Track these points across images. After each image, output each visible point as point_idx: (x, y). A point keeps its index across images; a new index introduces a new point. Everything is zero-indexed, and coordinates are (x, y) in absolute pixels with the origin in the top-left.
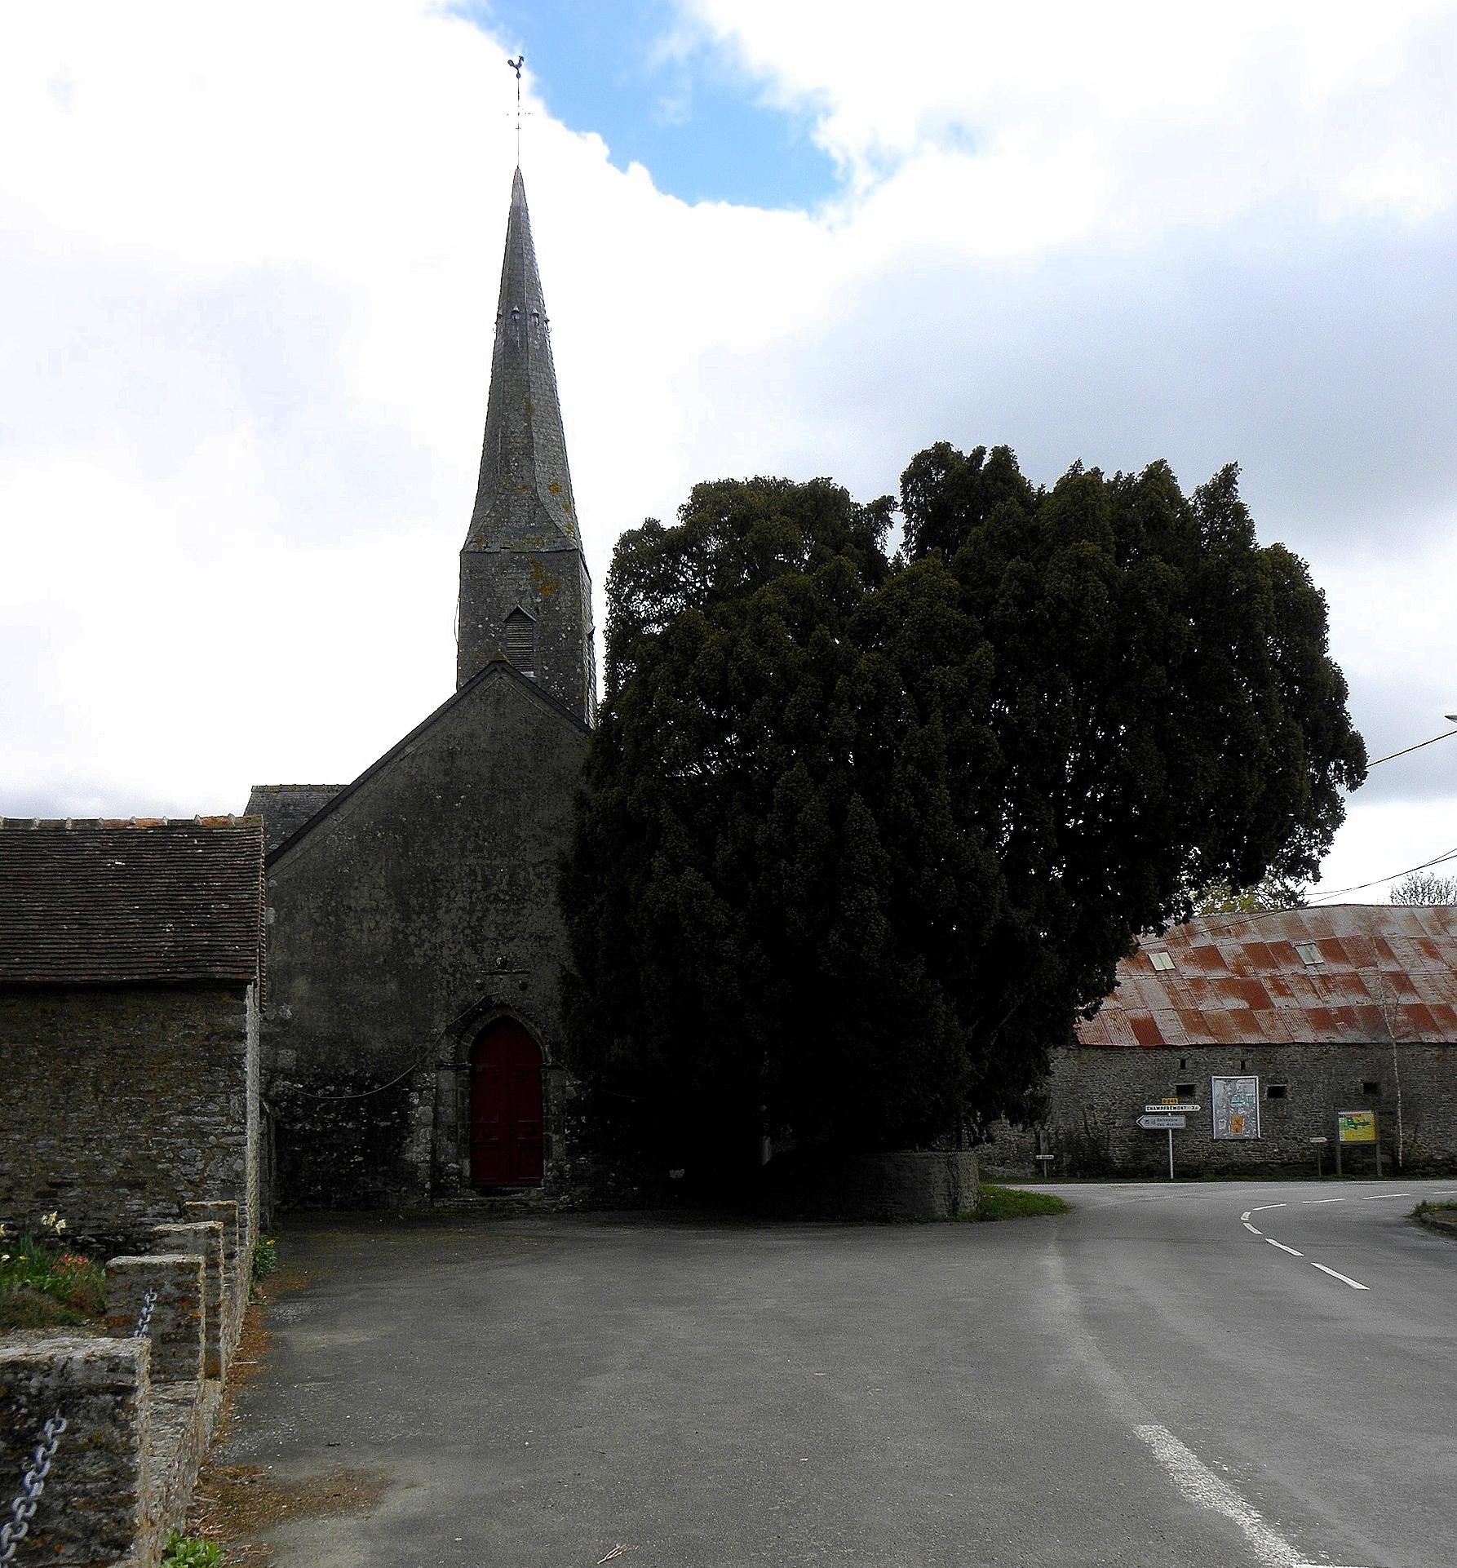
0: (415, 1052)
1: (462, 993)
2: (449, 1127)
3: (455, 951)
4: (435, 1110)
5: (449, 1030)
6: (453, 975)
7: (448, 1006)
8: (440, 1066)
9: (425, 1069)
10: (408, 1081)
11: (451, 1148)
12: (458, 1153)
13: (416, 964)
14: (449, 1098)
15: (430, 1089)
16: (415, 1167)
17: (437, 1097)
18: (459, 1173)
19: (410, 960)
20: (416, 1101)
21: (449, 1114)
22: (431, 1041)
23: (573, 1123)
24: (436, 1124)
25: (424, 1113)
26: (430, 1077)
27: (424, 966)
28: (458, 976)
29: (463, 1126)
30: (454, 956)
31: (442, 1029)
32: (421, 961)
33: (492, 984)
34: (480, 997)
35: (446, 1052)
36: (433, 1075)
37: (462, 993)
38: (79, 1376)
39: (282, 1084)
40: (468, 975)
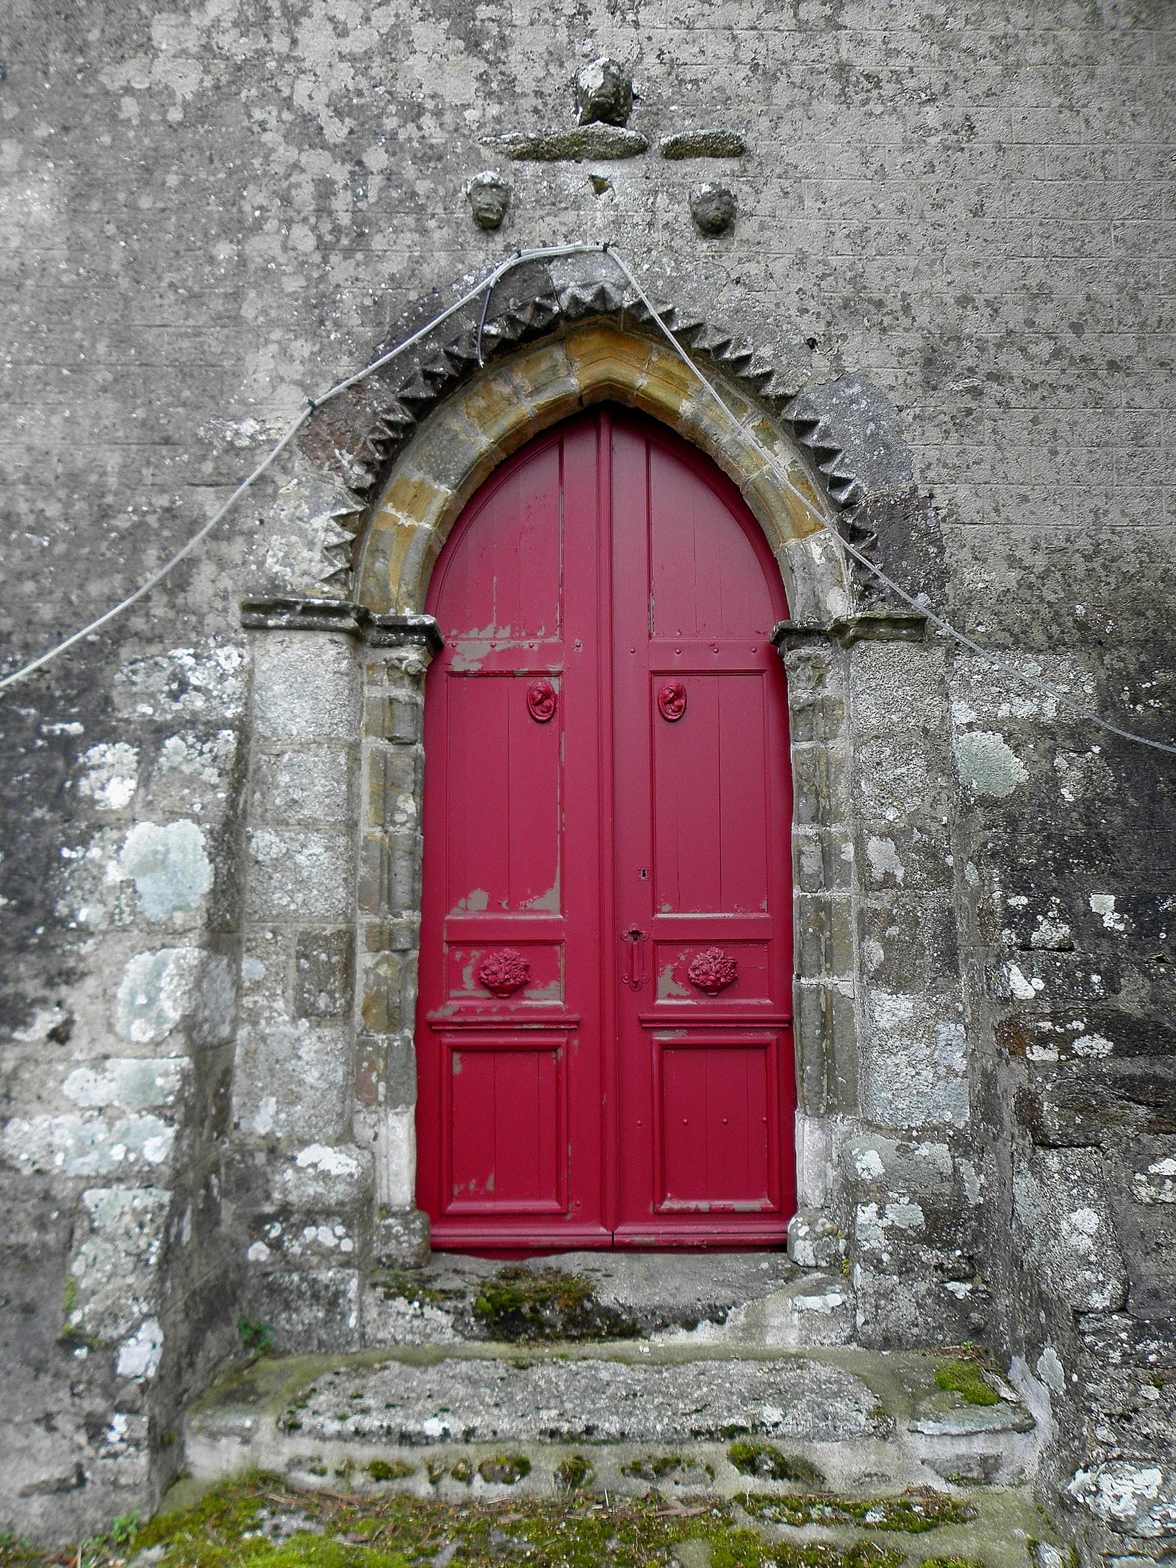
0: (136, 537)
1: (394, 249)
2: (308, 941)
3: (361, 40)
4: (228, 840)
5: (322, 427)
6: (351, 154)
7: (318, 309)
8: (267, 610)
9: (187, 627)
10: (84, 691)
11: (314, 1057)
12: (357, 1088)
13: (157, 96)
14: (307, 781)
15: (209, 730)
16: (62, 1216)
17: (240, 772)
18: (361, 1209)
19: (132, 73)
20: (117, 793)
21: (306, 872)
22: (220, 482)
23: (1049, 932)
24: (225, 927)
25: (155, 863)
26: (217, 668)
27: (201, 112)
28: (376, 158)
29: (382, 940)
30: (359, 61)
31: (287, 417)
32: (187, 82)
33: (555, 201)
34: (486, 264)
35: (299, 545)
36: (229, 658)
37: (394, 249)
38: (277, 1178)
39: (490, 1185)
40: (430, 156)
